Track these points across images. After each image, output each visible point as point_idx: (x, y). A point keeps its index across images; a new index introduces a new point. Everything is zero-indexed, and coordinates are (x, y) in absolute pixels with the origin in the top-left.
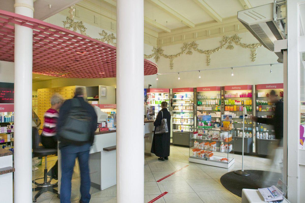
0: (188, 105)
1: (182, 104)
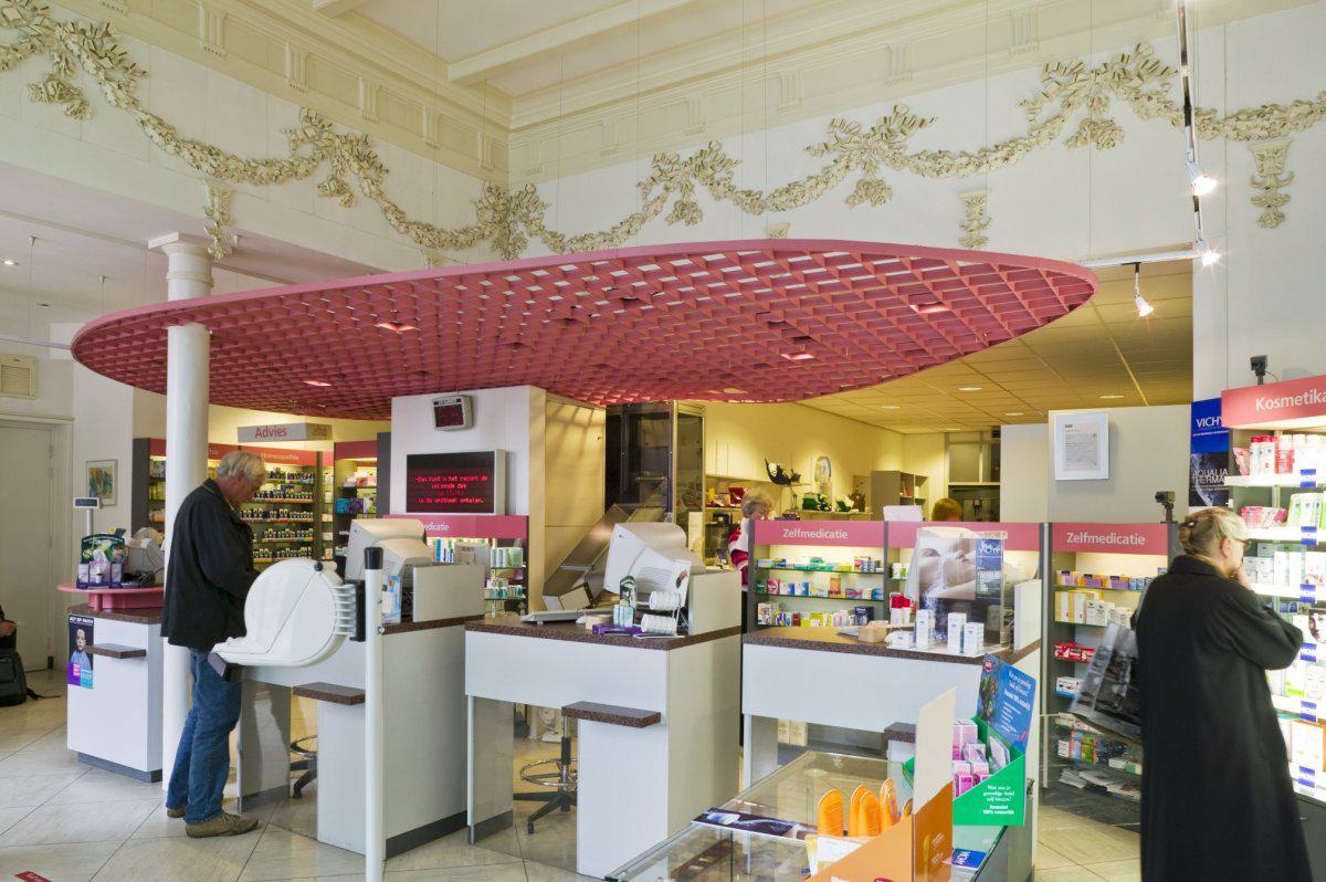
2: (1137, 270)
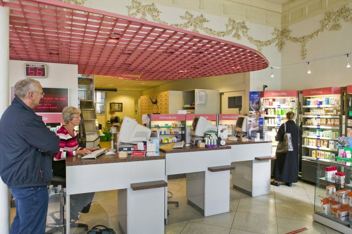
0: (330, 117)
1: (319, 115)
2: (308, 64)
